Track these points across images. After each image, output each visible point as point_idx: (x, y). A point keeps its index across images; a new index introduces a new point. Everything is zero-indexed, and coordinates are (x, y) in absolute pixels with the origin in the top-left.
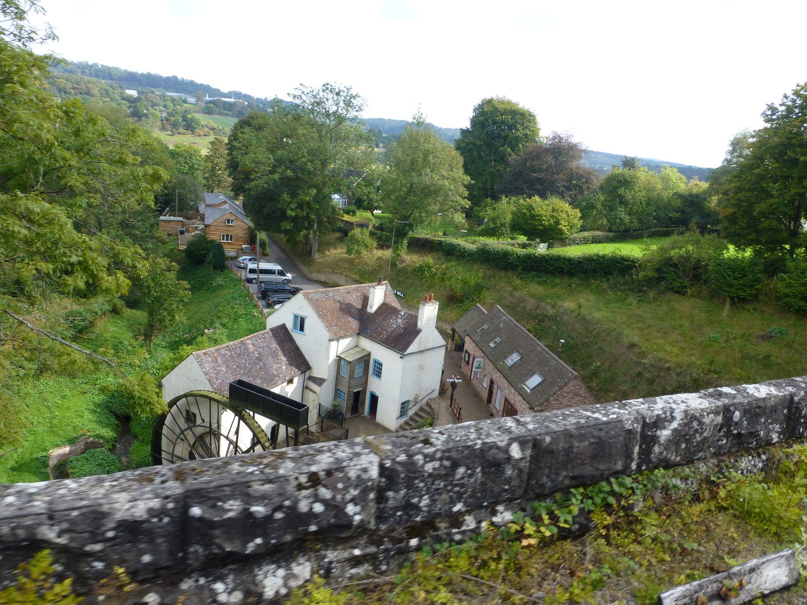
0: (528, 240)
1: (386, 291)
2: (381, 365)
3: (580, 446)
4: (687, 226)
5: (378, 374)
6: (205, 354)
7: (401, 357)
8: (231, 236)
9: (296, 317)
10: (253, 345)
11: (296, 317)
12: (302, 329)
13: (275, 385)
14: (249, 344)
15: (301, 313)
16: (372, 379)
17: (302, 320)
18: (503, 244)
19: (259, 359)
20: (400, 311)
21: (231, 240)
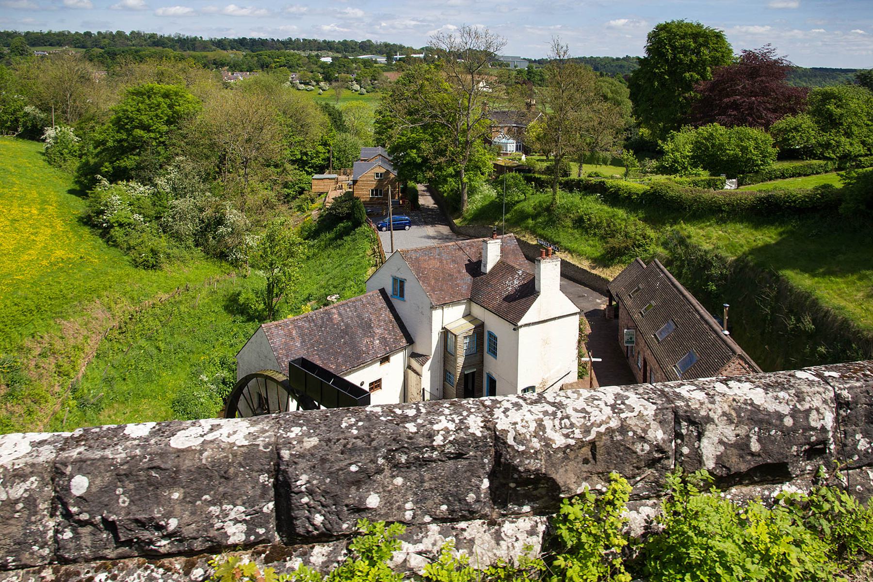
0: (711, 175)
1: (502, 246)
2: (496, 338)
3: (800, 71)
4: (622, 424)
5: (494, 352)
6: (276, 327)
7: (514, 329)
8: (381, 191)
9: (395, 279)
10: (340, 314)
11: (395, 279)
12: (402, 295)
13: (359, 363)
14: (334, 313)
15: (400, 276)
16: (488, 357)
17: (402, 282)
18: (770, 377)
19: (345, 332)
20: (518, 270)
21: (381, 195)
